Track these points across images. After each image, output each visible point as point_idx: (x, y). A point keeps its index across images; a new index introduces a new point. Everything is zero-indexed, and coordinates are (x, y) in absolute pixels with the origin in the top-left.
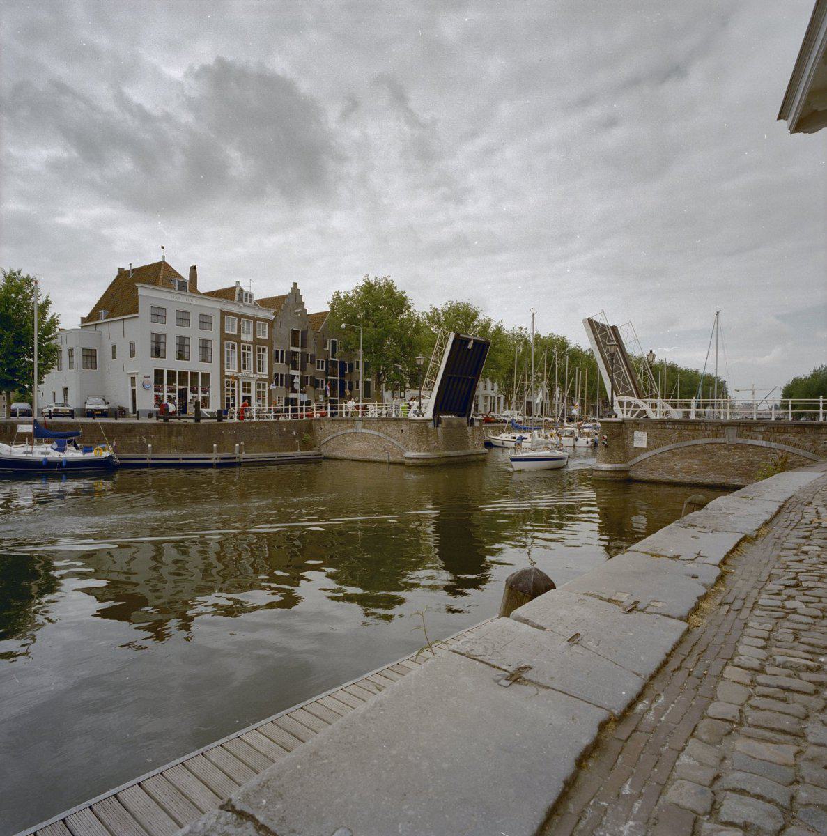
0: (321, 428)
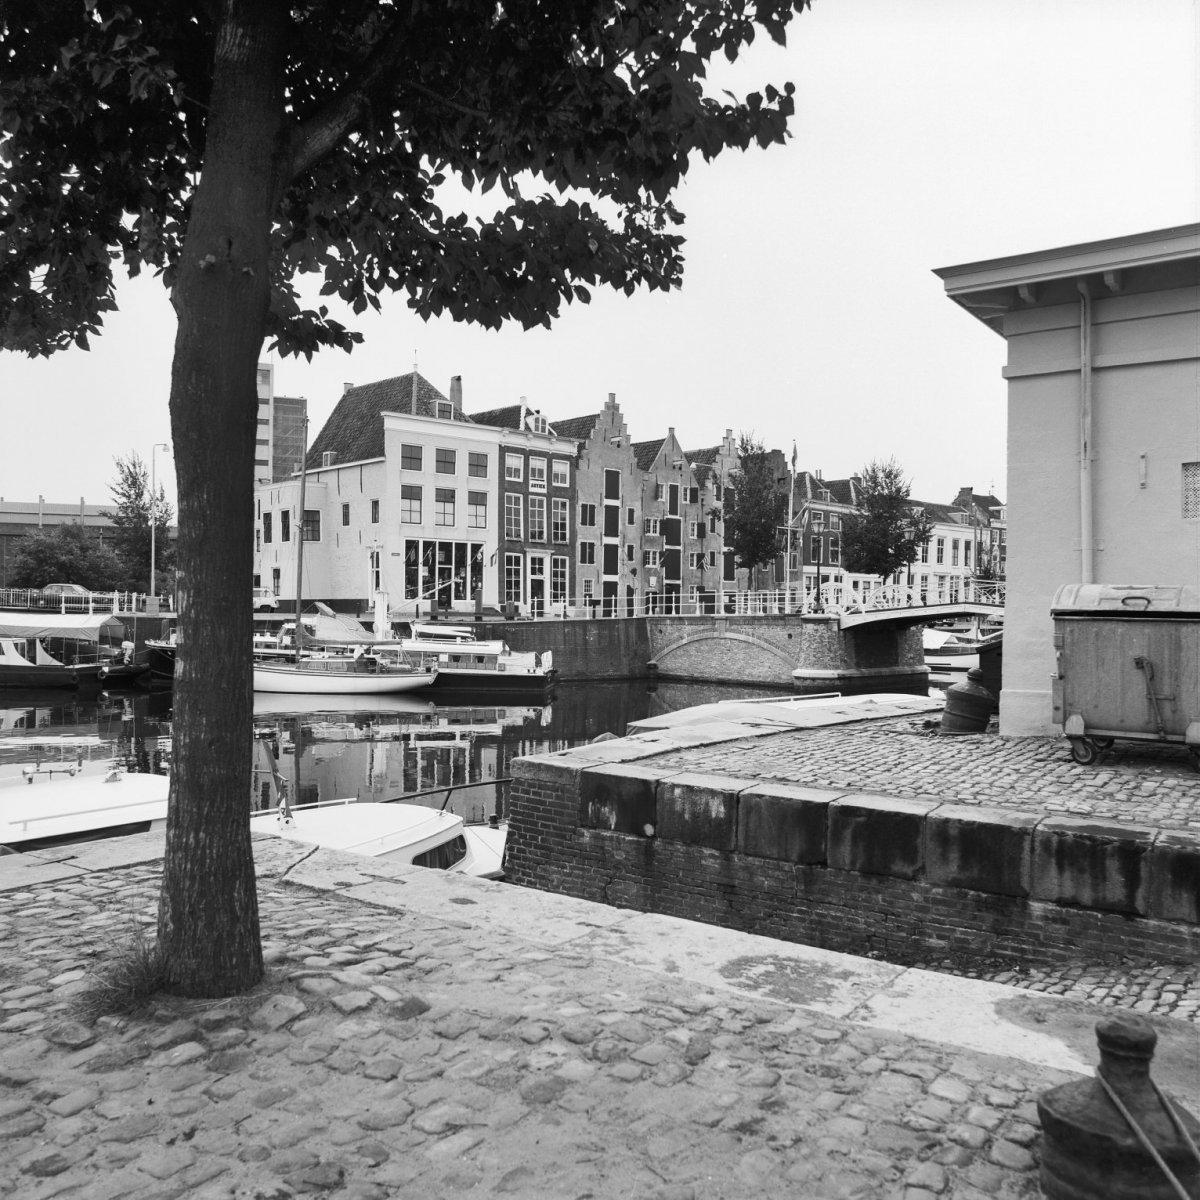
0: (661, 631)
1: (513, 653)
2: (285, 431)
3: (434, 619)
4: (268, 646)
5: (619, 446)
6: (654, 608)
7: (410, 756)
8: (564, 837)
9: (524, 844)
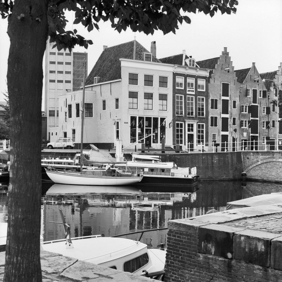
0: (248, 158)
1: (178, 168)
2: (78, 67)
3: (143, 152)
4: (69, 164)
5: (228, 72)
6: (245, 147)
7: (132, 213)
8: (191, 257)
9: (173, 260)
